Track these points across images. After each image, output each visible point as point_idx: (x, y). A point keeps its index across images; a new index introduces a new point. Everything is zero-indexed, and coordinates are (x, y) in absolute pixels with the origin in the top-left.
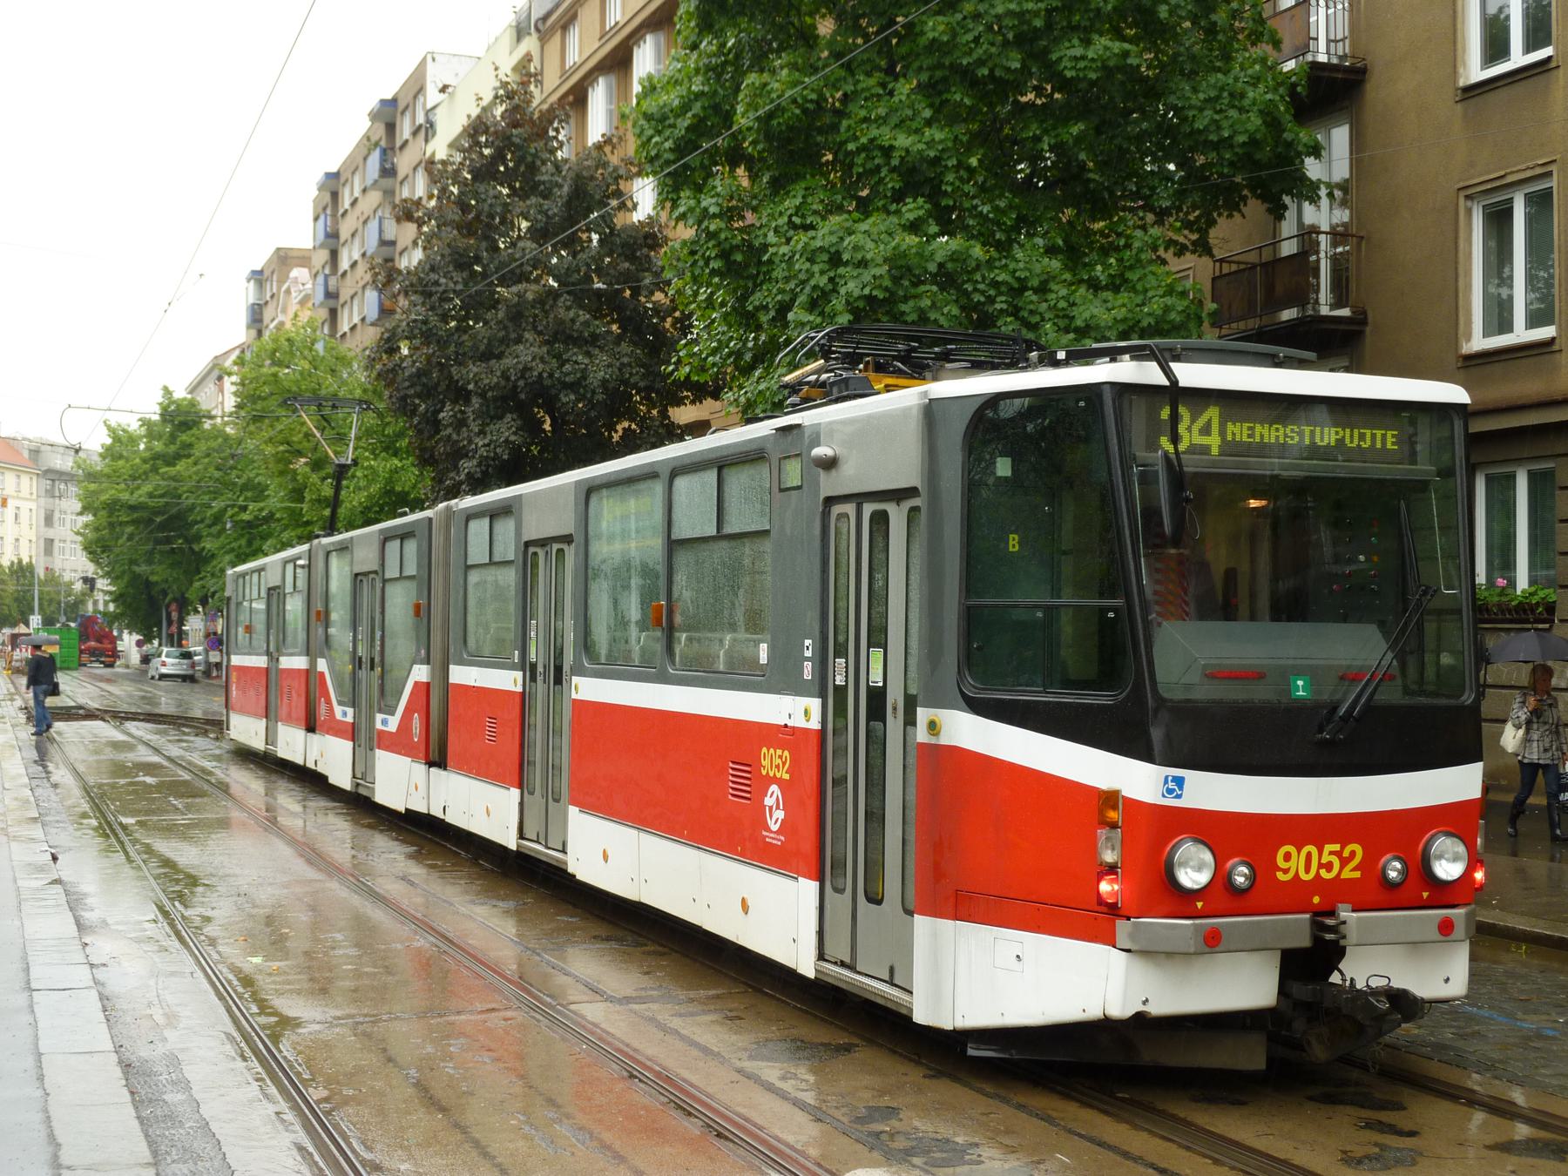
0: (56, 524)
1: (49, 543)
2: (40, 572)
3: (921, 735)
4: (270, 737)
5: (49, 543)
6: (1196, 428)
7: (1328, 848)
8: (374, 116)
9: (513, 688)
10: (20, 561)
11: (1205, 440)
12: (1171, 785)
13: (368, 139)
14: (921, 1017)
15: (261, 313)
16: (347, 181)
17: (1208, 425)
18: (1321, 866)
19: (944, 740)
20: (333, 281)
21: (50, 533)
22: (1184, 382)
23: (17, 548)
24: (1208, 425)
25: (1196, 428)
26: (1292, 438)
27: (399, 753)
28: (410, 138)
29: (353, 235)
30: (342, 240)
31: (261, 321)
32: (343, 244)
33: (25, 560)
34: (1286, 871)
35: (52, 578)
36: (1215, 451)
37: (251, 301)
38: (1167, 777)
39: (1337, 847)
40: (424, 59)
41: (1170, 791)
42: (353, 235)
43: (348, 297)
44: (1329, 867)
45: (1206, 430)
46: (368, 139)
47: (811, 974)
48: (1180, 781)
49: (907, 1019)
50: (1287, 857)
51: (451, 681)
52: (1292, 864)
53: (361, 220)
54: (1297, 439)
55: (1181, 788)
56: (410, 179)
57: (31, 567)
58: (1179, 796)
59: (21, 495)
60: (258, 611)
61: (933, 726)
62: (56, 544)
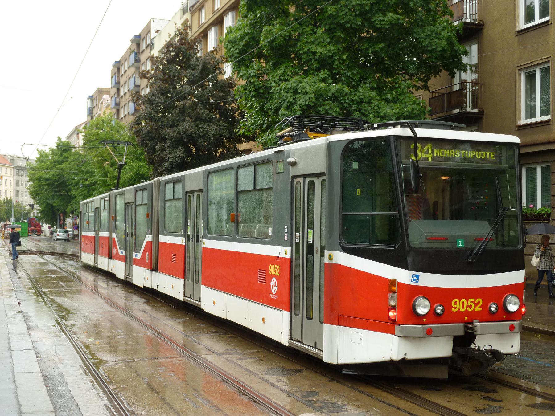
0: (20, 185)
1: (17, 192)
2: (14, 202)
3: (326, 260)
4: (96, 261)
5: (17, 192)
6: (423, 151)
7: (470, 300)
8: (132, 41)
9: (181, 244)
10: (7, 199)
11: (426, 156)
12: (415, 278)
13: (130, 49)
14: (326, 360)
15: (92, 111)
16: (123, 64)
17: (428, 150)
18: (467, 306)
19: (334, 262)
20: (118, 100)
21: (18, 189)
22: (419, 135)
23: (6, 194)
24: (428, 150)
25: (423, 151)
26: (457, 155)
28: (145, 49)
29: (125, 83)
30: (121, 85)
31: (92, 113)
32: (122, 86)
33: (9, 198)
34: (455, 308)
35: (18, 204)
36: (430, 159)
37: (89, 106)
38: (413, 275)
39: (473, 300)
40: (150, 21)
41: (414, 280)
42: (125, 83)
43: (123, 105)
44: (470, 307)
45: (427, 152)
46: (130, 49)
47: (287, 345)
48: (418, 276)
49: (321, 361)
50: (456, 303)
51: (160, 241)
52: (457, 306)
53: (128, 78)
54: (459, 155)
55: (418, 279)
56: (145, 63)
57: (11, 201)
58: (417, 282)
61: (330, 257)
62: (20, 192)
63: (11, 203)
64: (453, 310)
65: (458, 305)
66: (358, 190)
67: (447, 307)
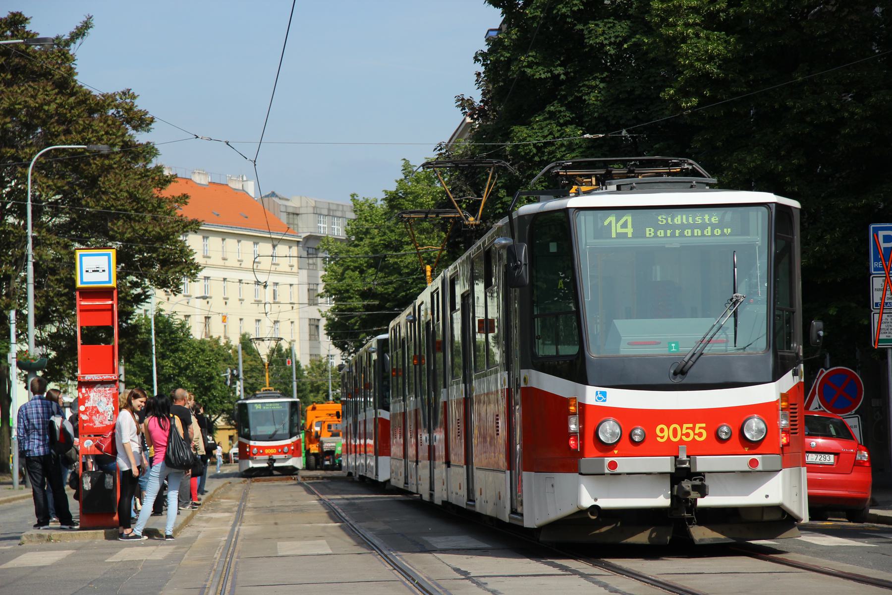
4: (879, 290)
7: (685, 426)
11: (624, 230)
12: (600, 396)
14: (525, 526)
17: (626, 223)
18: (682, 435)
19: (529, 385)
24: (626, 223)
26: (662, 218)
27: (636, 558)
34: (662, 438)
36: (630, 235)
38: (597, 392)
39: (691, 425)
41: (600, 399)
44: (687, 435)
45: (625, 225)
47: (507, 520)
48: (604, 394)
49: (522, 527)
50: (662, 430)
52: (666, 433)
54: (665, 221)
55: (605, 397)
58: (605, 401)
59: (227, 263)
60: (370, 445)
63: (163, 284)
64: (659, 439)
65: (664, 433)
66: (648, 229)
67: (648, 435)
